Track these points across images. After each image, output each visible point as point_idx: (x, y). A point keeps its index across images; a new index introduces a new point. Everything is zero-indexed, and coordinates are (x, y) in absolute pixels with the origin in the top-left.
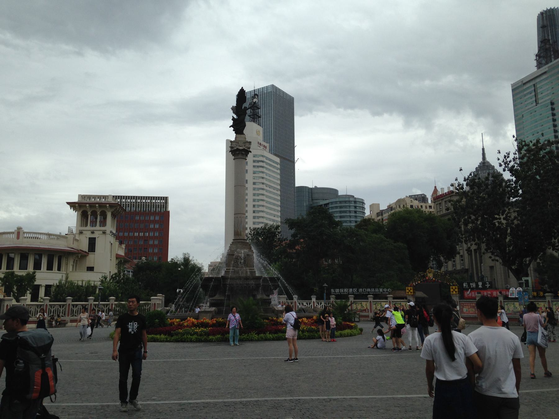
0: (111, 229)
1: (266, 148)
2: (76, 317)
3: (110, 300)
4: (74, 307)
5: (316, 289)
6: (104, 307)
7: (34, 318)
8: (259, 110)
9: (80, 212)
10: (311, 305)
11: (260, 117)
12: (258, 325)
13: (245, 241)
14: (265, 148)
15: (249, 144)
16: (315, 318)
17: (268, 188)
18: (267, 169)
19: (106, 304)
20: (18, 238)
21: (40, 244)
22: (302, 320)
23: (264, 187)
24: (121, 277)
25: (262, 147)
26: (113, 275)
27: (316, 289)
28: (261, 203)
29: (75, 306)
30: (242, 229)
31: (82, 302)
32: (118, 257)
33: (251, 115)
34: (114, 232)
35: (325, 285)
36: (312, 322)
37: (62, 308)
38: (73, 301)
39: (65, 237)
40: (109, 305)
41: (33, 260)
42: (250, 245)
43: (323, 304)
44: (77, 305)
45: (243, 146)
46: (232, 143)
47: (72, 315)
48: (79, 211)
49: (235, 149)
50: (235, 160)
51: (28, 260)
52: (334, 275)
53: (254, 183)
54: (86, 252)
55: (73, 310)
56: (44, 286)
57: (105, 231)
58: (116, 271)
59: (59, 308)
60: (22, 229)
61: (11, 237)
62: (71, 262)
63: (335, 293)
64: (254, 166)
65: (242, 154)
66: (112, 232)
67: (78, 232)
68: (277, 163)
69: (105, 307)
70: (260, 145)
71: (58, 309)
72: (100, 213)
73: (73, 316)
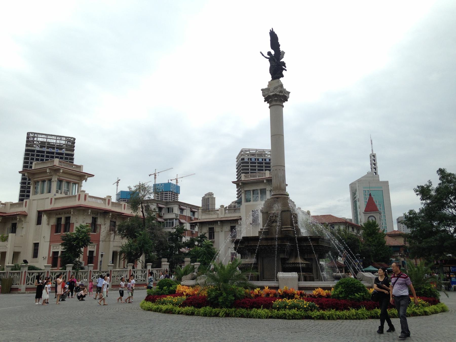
4: (30, 275)
10: (145, 272)
31: (17, 270)
40: (66, 273)
44: (14, 273)
50: (271, 107)
55: (29, 278)
59: (82, 275)
65: (276, 101)
69: (158, 272)
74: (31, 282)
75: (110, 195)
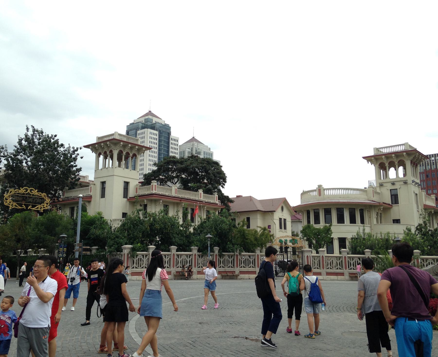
0: (413, 179)
2: (354, 271)
3: (193, 250)
7: (335, 270)
19: (145, 254)
20: (320, 194)
21: (340, 199)
24: (427, 228)
26: (417, 226)
32: (426, 208)
34: (418, 181)
37: (231, 258)
39: (364, 191)
42: (172, 166)
54: (389, 204)
56: (336, 239)
57: (406, 181)
58: (421, 222)
60: (322, 186)
61: (315, 195)
66: (414, 182)
67: (378, 185)
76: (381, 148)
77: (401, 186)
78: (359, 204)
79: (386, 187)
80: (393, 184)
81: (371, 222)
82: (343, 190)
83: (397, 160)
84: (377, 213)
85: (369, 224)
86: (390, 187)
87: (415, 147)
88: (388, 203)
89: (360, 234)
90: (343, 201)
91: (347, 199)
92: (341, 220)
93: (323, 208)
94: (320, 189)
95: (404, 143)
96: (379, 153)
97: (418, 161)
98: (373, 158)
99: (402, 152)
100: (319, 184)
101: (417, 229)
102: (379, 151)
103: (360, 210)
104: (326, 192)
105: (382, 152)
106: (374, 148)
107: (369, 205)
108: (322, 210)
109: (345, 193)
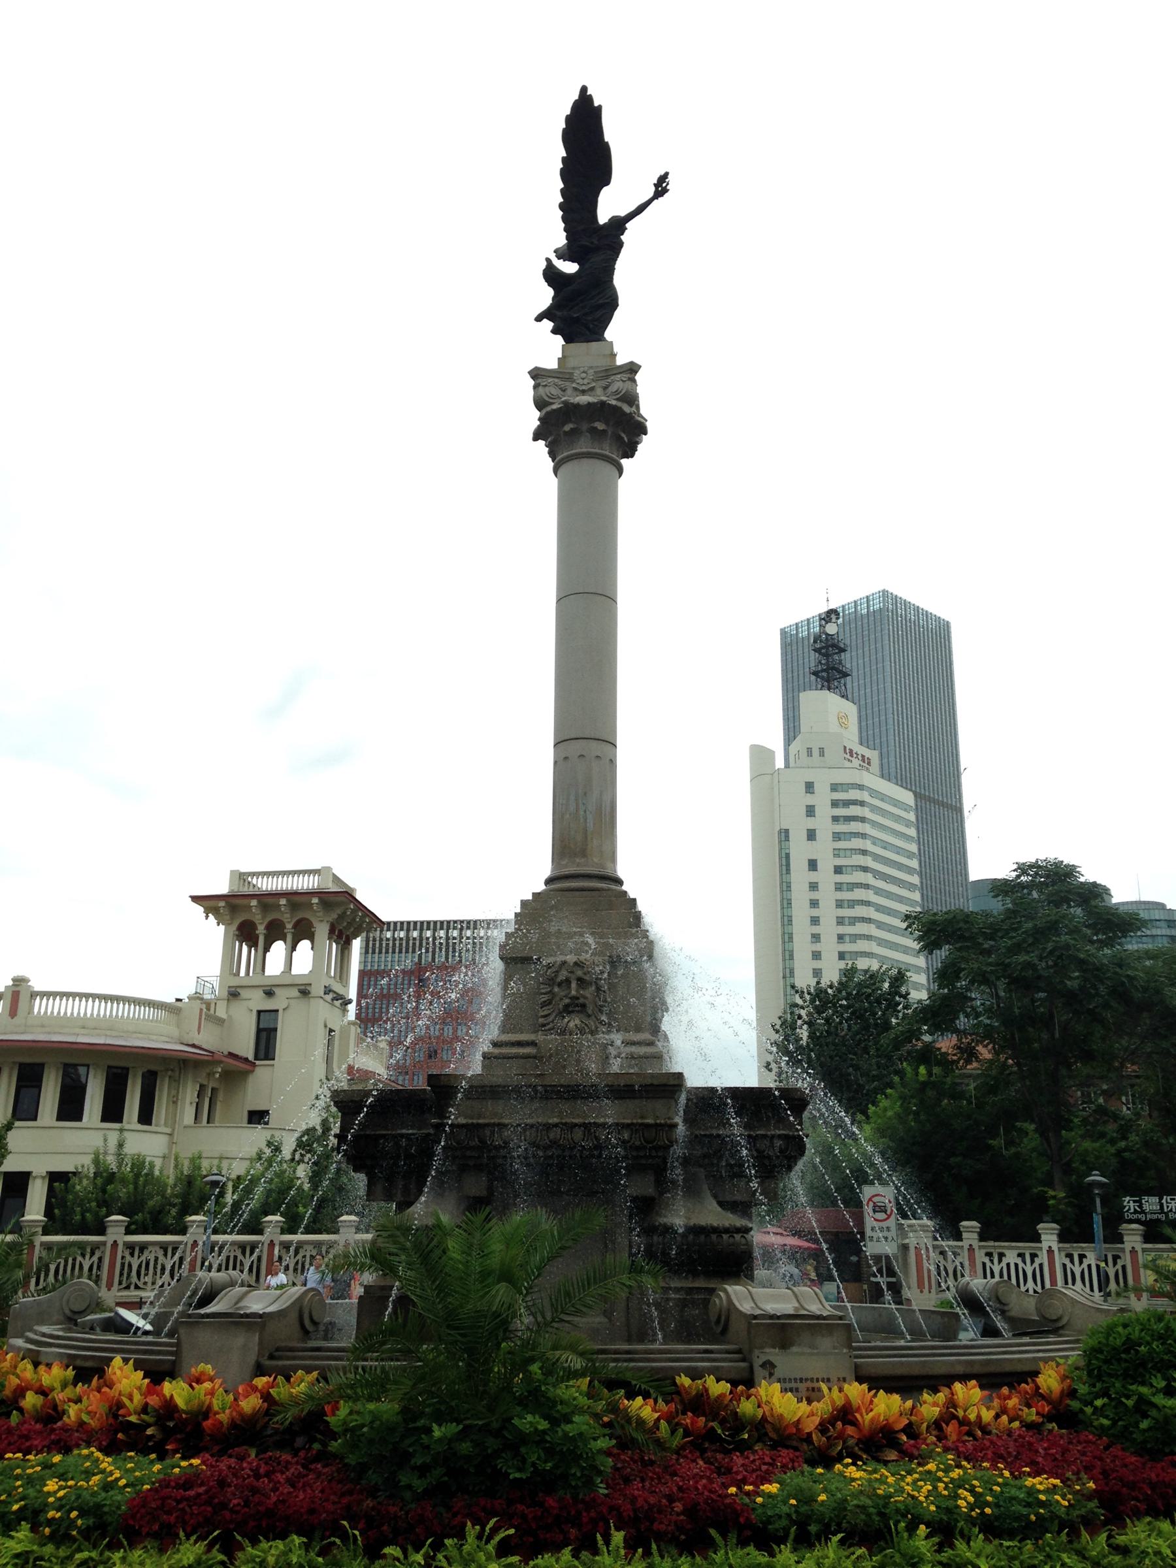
1: (869, 763)
5: (1057, 1194)
6: (165, 1255)
8: (848, 654)
9: (234, 927)
11: (845, 675)
12: (533, 1456)
13: (614, 887)
14: (865, 765)
15: (625, 376)
16: (1050, 1380)
17: (880, 884)
18: (874, 824)
19: (249, 1243)
20: (13, 1011)
22: (952, 1403)
23: (869, 878)
25: (856, 762)
27: (1057, 1194)
28: (861, 928)
29: (89, 1250)
30: (590, 817)
33: (819, 672)
35: (1096, 1177)
36: (1031, 1415)
38: (128, 1232)
39: (173, 1009)
41: (56, 1083)
43: (1091, 1259)
44: (143, 1247)
45: (599, 391)
46: (539, 381)
47: (124, 1285)
48: (229, 924)
49: (555, 407)
50: (560, 472)
51: (39, 1087)
52: (1123, 1144)
53: (838, 870)
54: (246, 1059)
59: (240, 1257)
62: (189, 1091)
63: (1143, 1212)
64: (835, 819)
65: (597, 435)
66: (330, 991)
67: (225, 994)
68: (906, 807)
70: (852, 756)
71: (156, 1259)
72: (295, 927)
73: (128, 1288)
74: (169, 1279)
75: (804, 810)
76: (253, 874)
77: (292, 1001)
78: (137, 1054)
79: (247, 1002)
80: (269, 993)
81: (175, 1116)
82: (100, 1002)
83: (292, 918)
84: (202, 1086)
85: (166, 1125)
86: (258, 1001)
87: (351, 885)
88: (245, 1056)
89: (105, 1161)
90: (102, 1042)
91: (108, 1033)
92: (70, 1109)
93: (14, 1063)
94: (19, 992)
95: (319, 867)
96: (245, 890)
97: (352, 929)
98: (222, 904)
99: (310, 894)
100: (20, 973)
101: (300, 1144)
102: (246, 884)
103: (143, 1076)
104: (40, 1006)
105: (254, 886)
106: (232, 872)
107: (179, 1060)
108: (11, 1069)
109: (102, 1013)
